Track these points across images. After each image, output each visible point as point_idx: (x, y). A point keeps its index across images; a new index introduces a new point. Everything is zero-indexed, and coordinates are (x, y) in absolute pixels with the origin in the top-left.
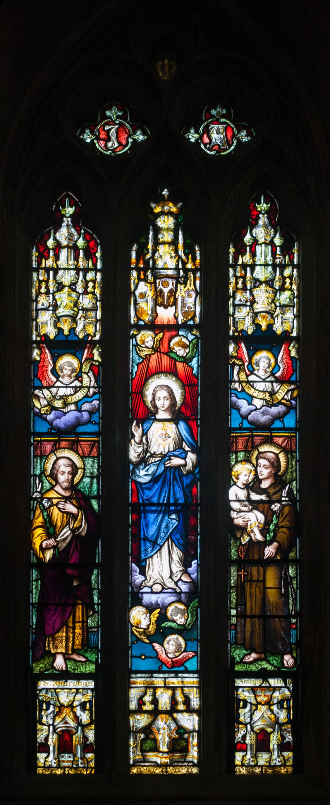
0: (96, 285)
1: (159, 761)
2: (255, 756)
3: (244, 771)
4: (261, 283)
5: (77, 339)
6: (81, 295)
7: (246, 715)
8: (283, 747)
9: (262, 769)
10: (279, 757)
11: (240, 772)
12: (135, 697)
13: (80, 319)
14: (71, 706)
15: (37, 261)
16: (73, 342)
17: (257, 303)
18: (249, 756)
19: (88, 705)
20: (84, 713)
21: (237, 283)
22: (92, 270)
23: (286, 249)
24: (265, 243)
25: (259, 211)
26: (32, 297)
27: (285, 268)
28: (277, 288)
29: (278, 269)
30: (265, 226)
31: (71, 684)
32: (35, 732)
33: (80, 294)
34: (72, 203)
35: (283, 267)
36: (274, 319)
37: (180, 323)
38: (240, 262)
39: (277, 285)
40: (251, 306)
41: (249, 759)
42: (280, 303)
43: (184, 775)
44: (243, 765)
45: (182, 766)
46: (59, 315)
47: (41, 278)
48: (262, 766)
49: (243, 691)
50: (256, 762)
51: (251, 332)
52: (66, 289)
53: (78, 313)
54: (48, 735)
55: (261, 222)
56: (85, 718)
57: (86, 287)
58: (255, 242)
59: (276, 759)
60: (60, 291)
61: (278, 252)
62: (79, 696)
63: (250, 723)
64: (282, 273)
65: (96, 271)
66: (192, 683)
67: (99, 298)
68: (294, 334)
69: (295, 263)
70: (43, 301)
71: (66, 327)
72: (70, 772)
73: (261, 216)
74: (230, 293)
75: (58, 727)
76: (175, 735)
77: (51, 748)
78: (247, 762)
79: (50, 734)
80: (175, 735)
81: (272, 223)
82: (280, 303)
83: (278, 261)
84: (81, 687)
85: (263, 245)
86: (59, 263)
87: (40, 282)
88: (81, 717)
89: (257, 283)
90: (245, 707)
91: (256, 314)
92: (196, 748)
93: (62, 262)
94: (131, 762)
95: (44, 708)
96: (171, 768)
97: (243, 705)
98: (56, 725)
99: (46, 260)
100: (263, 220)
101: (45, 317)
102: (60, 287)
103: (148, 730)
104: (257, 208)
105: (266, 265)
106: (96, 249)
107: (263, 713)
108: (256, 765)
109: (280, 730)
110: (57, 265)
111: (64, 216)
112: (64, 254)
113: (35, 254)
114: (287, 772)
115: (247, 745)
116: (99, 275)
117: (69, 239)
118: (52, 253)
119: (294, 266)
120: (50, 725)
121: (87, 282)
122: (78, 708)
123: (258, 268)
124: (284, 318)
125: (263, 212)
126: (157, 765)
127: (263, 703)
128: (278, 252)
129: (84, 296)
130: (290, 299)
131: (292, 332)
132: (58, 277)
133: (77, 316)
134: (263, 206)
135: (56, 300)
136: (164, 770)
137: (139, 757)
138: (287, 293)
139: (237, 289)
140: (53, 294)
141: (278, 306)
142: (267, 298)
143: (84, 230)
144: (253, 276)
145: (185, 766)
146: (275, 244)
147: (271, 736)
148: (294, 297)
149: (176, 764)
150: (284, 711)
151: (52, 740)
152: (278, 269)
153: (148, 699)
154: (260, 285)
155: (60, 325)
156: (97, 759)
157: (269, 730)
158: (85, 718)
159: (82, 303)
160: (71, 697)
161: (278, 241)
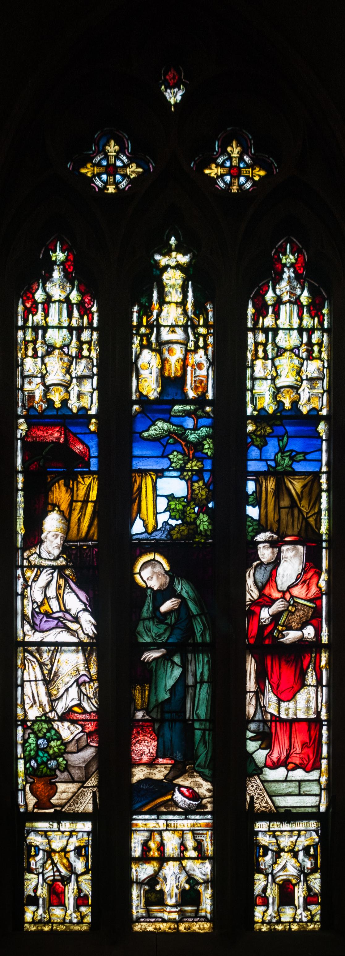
0: (92, 347)
3: (264, 928)
4: (285, 350)
5: (266, 414)
6: (75, 359)
8: (309, 900)
10: (75, 912)
12: (139, 843)
13: (303, 390)
14: (64, 850)
15: (253, 320)
16: (64, 417)
17: (50, 374)
18: (40, 911)
19: (312, 850)
20: (79, 859)
21: (320, 352)
22: (87, 328)
23: (199, 309)
24: (290, 302)
26: (17, 361)
27: (82, 331)
28: (74, 355)
31: (66, 826)
32: (252, 883)
33: (73, 358)
35: (80, 330)
36: (69, 393)
38: (30, 324)
40: (43, 377)
42: (307, 376)
44: (263, 922)
47: (29, 338)
50: (278, 918)
51: (272, 411)
52: (57, 352)
54: (266, 886)
55: (285, 276)
56: (79, 865)
57: (80, 349)
58: (48, 300)
62: (73, 840)
63: (271, 873)
65: (93, 329)
67: (95, 363)
68: (324, 412)
69: (326, 327)
71: (56, 397)
73: (286, 270)
74: (248, 362)
75: (278, 874)
77: (271, 901)
79: (269, 884)
81: (68, 277)
82: (307, 376)
84: (303, 829)
85: (288, 304)
87: (27, 342)
89: (51, 349)
90: (265, 854)
91: (278, 390)
95: (261, 854)
98: (276, 874)
103: (153, 880)
104: (281, 260)
105: (60, 327)
107: (287, 861)
108: (279, 922)
109: (306, 881)
110: (46, 322)
112: (54, 308)
113: (251, 310)
116: (95, 336)
117: (291, 293)
118: (40, 307)
122: (72, 853)
130: (319, 369)
131: (90, 409)
134: (59, 256)
137: (142, 912)
139: (27, 356)
140: (273, 360)
143: (309, 282)
146: (70, 301)
147: (296, 888)
149: (142, 920)
150: (82, 859)
151: (43, 892)
152: (74, 332)
153: (153, 845)
154: (284, 352)
155: (280, 398)
157: (294, 881)
158: (79, 865)
159: (307, 371)
160: (64, 842)
161: (75, 297)
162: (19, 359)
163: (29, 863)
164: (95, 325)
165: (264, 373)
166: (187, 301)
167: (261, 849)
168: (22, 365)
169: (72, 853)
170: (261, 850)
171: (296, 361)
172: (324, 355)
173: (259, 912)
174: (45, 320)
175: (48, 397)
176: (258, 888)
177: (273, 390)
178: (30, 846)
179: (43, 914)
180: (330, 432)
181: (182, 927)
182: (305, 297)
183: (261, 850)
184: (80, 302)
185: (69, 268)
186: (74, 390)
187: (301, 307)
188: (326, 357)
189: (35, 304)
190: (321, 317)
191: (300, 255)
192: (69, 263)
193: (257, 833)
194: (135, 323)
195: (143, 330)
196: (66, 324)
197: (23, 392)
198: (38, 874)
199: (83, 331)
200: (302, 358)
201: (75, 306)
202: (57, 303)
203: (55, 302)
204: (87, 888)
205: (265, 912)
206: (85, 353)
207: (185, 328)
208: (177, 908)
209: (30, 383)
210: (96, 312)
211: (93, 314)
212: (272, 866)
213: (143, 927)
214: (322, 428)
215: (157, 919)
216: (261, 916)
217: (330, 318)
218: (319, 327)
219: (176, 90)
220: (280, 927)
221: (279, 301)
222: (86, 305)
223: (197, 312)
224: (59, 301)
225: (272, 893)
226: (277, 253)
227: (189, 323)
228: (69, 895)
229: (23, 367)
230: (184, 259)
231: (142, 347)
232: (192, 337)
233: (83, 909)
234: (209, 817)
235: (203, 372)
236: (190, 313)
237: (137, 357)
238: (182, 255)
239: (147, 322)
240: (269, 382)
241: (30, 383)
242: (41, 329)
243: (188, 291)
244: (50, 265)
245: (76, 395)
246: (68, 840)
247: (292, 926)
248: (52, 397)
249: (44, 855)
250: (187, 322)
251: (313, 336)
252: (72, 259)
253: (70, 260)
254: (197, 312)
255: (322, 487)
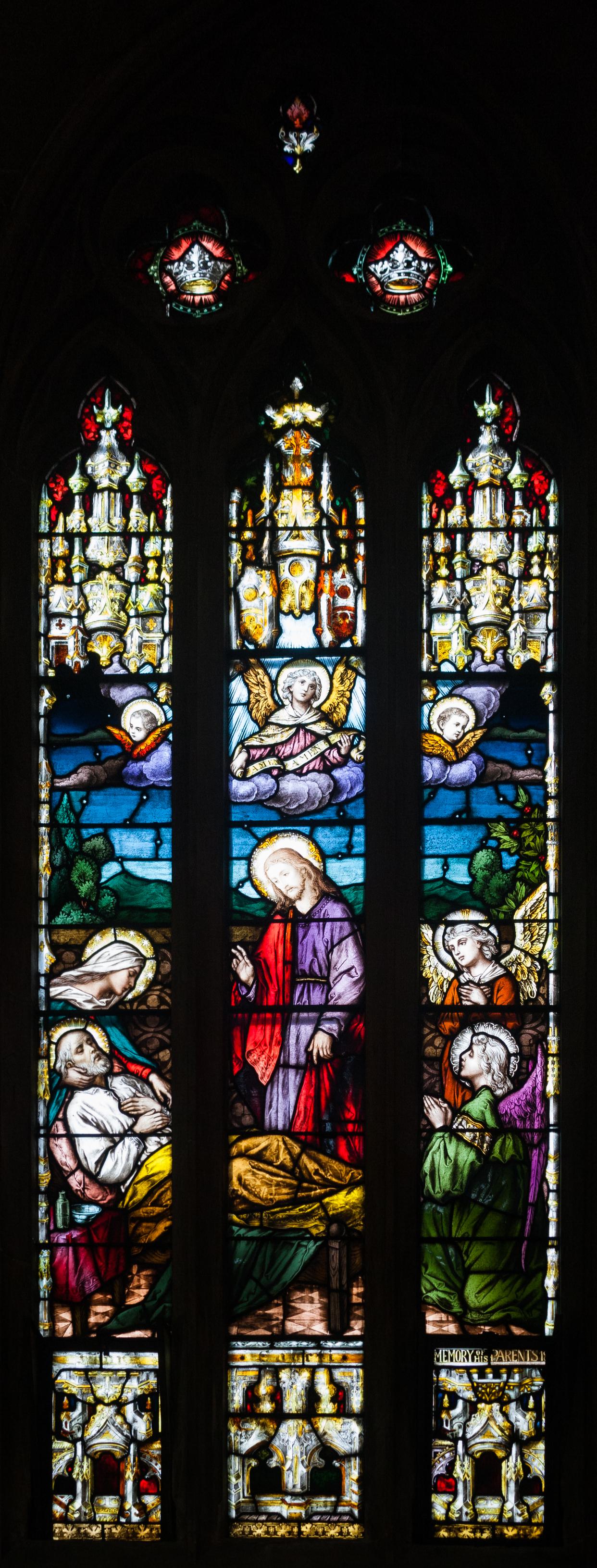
1: (285, 1511)
2: (92, 1503)
6: (517, 581)
7: (454, 1422)
9: (103, 1529)
11: (62, 1533)
13: (515, 629)
14: (119, 1405)
18: (511, 1503)
20: (142, 1416)
22: (155, 534)
24: (491, 485)
25: (99, 423)
27: (531, 535)
28: (516, 575)
29: (517, 537)
30: (494, 447)
32: (48, 1454)
34: (499, 393)
35: (526, 532)
37: (326, 645)
38: (60, 529)
39: (131, 574)
41: (461, 1510)
43: (259, 1539)
45: (256, 1521)
46: (476, 621)
48: (103, 1523)
49: (449, 1374)
53: (512, 617)
57: (144, 570)
58: (91, 489)
59: (512, 1510)
60: (94, 578)
61: (518, 501)
62: (133, 1383)
64: (524, 545)
65: (163, 534)
66: (280, 1359)
67: (167, 592)
68: (550, 666)
69: (552, 524)
70: (440, 593)
71: (102, 649)
72: (114, 1530)
75: (473, 1443)
76: (320, 1462)
78: (457, 1515)
80: (320, 1462)
81: (504, 444)
83: (517, 520)
85: (488, 489)
86: (474, 519)
88: (135, 1426)
89: (94, 569)
91: (89, 633)
92: (355, 1488)
93: (480, 517)
94: (233, 1514)
95: (446, 1404)
96: (309, 1526)
97: (70, 1404)
99: (448, 511)
100: (108, 438)
101: (443, 626)
102: (94, 569)
103: (263, 1450)
105: (494, 530)
106: (163, 491)
108: (93, 1522)
111: (482, 421)
112: (100, 503)
113: (46, 503)
114: (150, 1535)
115: (456, 1481)
116: (552, 543)
118: (459, 500)
119: (548, 530)
120: (78, 1440)
121: (528, 556)
123: (94, 540)
124: (529, 635)
125: (489, 420)
126: (279, 1519)
127: (106, 1401)
128: (518, 501)
129: (141, 588)
130: (156, 601)
132: (473, 546)
133: (509, 624)
135: (85, 597)
136: (296, 1530)
138: (152, 588)
140: (80, 585)
141: (516, 612)
142: (112, 601)
144: (85, 555)
145: (262, 1522)
147: (504, 1464)
148: (165, 596)
150: (529, 1415)
153: (264, 1389)
156: (166, 1505)
157: (500, 1454)
161: (516, 474)
162: (425, 583)
163: (59, 1422)
164: (168, 527)
165: (65, 607)
166: (320, 486)
167: (446, 1396)
168: (47, 596)
169: (513, 1405)
170: (446, 1398)
171: (501, 580)
172: (165, 576)
173: (439, 1504)
174: (86, 521)
175: (89, 649)
176: (59, 1466)
177: (465, 630)
178: (61, 1395)
179: (515, 1508)
180: (558, 699)
181: (306, 1528)
182: (134, 480)
183: (446, 1398)
184: (526, 484)
185: (126, 432)
186: (133, 637)
187: (509, 492)
188: (552, 575)
189: (69, 496)
190: (161, 512)
191: (127, 409)
192: (126, 424)
193: (438, 1369)
194: (234, 524)
195: (248, 535)
196: (502, 524)
197: (47, 641)
198: (74, 1442)
199: (531, 534)
200: (512, 577)
201: (517, 493)
202: (106, 493)
203: (102, 490)
204: (538, 1465)
205: (449, 1504)
206: (151, 575)
207: (317, 529)
208: (303, 1498)
209: (60, 626)
210: (554, 502)
211: (547, 504)
212: (465, 1426)
213: (247, 1530)
214: (547, 692)
215: (324, 1517)
216: (443, 1511)
217: (174, 513)
218: (157, 529)
219: (304, 134)
220: (95, 1532)
221: (472, 485)
222: (155, 495)
223: (338, 503)
224: (110, 489)
225: (463, 1471)
226: (89, 405)
227: (324, 523)
228: (508, 1476)
229: (48, 600)
230: (312, 414)
231: (246, 562)
232: (328, 546)
233: (531, 1500)
234: (360, 1344)
235: (349, 602)
236: (324, 504)
237: (237, 582)
238: (310, 407)
239: (254, 520)
240: (458, 616)
241: (60, 626)
242: (461, 533)
243: (321, 469)
244: (475, 425)
245: (519, 640)
246: (124, 1384)
247: (303, 1529)
248: (96, 650)
249: (465, 1408)
250: (320, 521)
251: (531, 540)
252: (130, 418)
253: (126, 420)
254: (338, 503)
255: (549, 790)
